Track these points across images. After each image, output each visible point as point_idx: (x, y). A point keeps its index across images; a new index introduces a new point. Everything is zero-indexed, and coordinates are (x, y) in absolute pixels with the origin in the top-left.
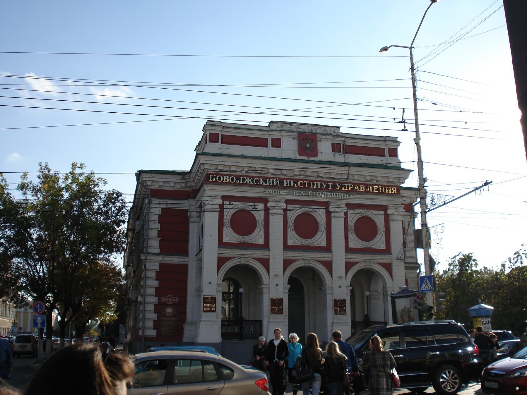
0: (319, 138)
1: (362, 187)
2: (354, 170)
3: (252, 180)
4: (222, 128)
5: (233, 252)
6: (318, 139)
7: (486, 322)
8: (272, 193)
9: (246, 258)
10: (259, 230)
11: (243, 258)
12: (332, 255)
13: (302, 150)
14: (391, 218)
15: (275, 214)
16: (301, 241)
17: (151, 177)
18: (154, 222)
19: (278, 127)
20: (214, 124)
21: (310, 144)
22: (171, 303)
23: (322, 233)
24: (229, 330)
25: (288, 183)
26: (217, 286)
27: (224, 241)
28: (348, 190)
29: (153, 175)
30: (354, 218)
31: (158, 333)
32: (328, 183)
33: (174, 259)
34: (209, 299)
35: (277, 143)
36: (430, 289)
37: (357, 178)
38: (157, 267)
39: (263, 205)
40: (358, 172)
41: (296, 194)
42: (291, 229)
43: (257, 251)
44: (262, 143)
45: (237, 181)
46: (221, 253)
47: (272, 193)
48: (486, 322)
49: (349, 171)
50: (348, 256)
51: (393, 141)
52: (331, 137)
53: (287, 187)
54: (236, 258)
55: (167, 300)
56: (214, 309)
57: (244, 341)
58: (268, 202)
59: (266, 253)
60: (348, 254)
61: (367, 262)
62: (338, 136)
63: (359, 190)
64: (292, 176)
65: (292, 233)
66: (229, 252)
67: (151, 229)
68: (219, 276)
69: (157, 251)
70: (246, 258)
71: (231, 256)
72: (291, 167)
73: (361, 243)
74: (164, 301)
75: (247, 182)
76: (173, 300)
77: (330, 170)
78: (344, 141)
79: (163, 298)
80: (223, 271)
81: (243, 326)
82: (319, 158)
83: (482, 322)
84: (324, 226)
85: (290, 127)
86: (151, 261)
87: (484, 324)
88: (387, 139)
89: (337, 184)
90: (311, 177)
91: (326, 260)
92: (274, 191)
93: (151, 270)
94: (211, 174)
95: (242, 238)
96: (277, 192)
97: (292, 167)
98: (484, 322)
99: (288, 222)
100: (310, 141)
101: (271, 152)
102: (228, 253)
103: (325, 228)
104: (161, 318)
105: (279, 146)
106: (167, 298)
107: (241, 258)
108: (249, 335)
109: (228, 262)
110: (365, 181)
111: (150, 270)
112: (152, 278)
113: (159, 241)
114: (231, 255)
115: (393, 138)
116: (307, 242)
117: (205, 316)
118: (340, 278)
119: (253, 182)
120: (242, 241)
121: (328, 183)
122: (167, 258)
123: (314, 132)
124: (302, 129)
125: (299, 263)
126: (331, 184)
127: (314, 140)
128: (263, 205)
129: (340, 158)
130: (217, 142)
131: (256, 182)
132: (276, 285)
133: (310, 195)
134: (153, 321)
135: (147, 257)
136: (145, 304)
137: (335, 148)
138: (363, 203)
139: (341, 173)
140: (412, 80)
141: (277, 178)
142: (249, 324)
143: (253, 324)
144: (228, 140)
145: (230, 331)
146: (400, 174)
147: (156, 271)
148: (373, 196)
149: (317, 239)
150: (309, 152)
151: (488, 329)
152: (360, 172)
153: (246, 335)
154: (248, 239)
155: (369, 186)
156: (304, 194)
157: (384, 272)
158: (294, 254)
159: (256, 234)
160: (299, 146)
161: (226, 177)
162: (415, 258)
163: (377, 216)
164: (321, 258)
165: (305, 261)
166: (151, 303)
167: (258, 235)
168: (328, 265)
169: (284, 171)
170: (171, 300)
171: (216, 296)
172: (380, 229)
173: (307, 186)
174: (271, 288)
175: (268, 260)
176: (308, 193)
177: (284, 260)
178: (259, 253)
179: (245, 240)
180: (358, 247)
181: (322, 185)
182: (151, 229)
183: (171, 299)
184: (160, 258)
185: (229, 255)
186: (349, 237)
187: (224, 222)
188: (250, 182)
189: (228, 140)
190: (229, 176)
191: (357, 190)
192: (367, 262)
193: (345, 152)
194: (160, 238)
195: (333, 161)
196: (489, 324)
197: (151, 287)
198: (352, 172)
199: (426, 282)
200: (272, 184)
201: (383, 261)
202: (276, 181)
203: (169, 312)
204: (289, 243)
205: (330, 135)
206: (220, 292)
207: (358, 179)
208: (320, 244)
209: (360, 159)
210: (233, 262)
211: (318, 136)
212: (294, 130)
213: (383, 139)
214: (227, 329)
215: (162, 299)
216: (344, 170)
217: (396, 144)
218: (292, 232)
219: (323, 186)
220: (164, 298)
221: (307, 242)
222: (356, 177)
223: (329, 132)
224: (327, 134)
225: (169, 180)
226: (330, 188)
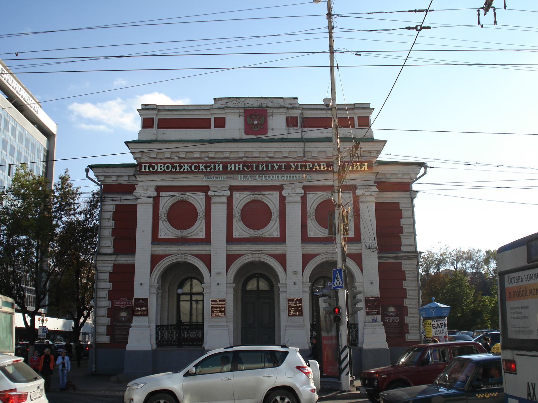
0: (269, 112)
1: (324, 165)
2: (310, 146)
3: (191, 167)
4: (157, 112)
5: (169, 248)
6: (269, 114)
7: (438, 324)
8: (212, 180)
9: (183, 254)
10: (200, 223)
11: (179, 255)
12: (286, 246)
13: (249, 128)
14: (213, 200)
15: (216, 203)
16: (249, 232)
17: (102, 172)
18: (108, 220)
19: (222, 104)
20: (149, 108)
21: (258, 120)
23: (274, 222)
24: (192, 335)
25: (358, 166)
26: (150, 287)
27: (159, 237)
28: (231, 171)
29: (105, 169)
30: (315, 203)
31: (111, 340)
32: (281, 164)
33: (128, 259)
34: (140, 302)
35: (221, 123)
36: (340, 285)
37: (316, 156)
38: (109, 268)
39: (278, 192)
40: (316, 148)
41: (241, 178)
42: (237, 219)
43: (196, 246)
44: (204, 124)
45: (173, 169)
46: (154, 250)
47: (212, 180)
48: (438, 324)
49: (304, 148)
50: (306, 247)
51: (365, 108)
52: (284, 110)
53: (231, 172)
54: (172, 256)
56: (146, 313)
58: (283, 189)
59: (207, 248)
60: (306, 245)
61: (330, 253)
62: (294, 108)
63: (205, 170)
64: (238, 159)
65: (238, 224)
66: (164, 248)
67: (105, 228)
68: (152, 277)
69: (111, 250)
70: (183, 254)
71: (167, 253)
72: (234, 149)
73: (323, 231)
75: (184, 169)
77: (281, 148)
78: (302, 114)
79: (116, 301)
80: (157, 270)
82: (270, 134)
83: (433, 325)
84: (277, 213)
85: (236, 103)
86: (104, 262)
87: (434, 327)
88: (356, 106)
89: (292, 164)
90: (260, 158)
91: (279, 253)
92: (215, 177)
93: (104, 272)
94: (144, 163)
95: (179, 232)
96: (218, 178)
97: (235, 148)
98: (434, 324)
99: (234, 211)
100: (258, 117)
101: (214, 133)
102: (163, 250)
103: (278, 216)
104: (114, 323)
105: (224, 126)
108: (163, 341)
109: (238, 260)
110: (327, 158)
112: (105, 281)
113: (112, 240)
114: (167, 252)
115: (364, 105)
116: (256, 233)
117: (135, 320)
118: (295, 273)
119: (191, 168)
120: (180, 235)
121: (281, 164)
122: (121, 258)
123: (265, 106)
124: (250, 104)
125: (247, 257)
126: (256, 165)
127: (262, 116)
128: (278, 192)
129: (295, 133)
130: (152, 127)
131: (195, 169)
132: (370, 283)
133: (257, 179)
134: (106, 326)
135: (97, 257)
136: (96, 308)
137: (291, 122)
138: (325, 184)
139: (280, 150)
140: (328, 29)
141: (220, 162)
142: (171, 329)
143: (167, 329)
144: (164, 124)
145: (193, 336)
146: (370, 146)
147: (110, 273)
148: (167, 177)
149: (268, 230)
150: (257, 129)
151: (441, 334)
152: (319, 148)
154: (186, 233)
155: (175, 165)
156: (251, 178)
157: (351, 264)
158: (240, 248)
159: (196, 227)
160: (245, 122)
161: (161, 166)
162: (414, 246)
163: (193, 197)
164: (273, 251)
165: (253, 255)
166: (104, 307)
167: (198, 227)
168: (282, 259)
169: (226, 154)
170: (125, 303)
171: (148, 298)
172: (165, 215)
173: (254, 169)
175: (360, 255)
176: (256, 177)
177: (302, 255)
178: (199, 248)
179: (183, 235)
180: (245, 237)
181: (273, 167)
182: (105, 228)
183: (124, 302)
184: (113, 258)
185: (165, 252)
186: (308, 224)
187: (159, 215)
188: (187, 169)
189: (164, 124)
190: (164, 164)
191: (316, 169)
192: (330, 253)
193: (303, 126)
194: (114, 237)
195: (286, 138)
196: (441, 327)
197: (103, 289)
198: (309, 148)
199: (338, 276)
200: (205, 169)
201: (350, 251)
202: (219, 165)
203: (123, 317)
204: (235, 236)
205: (284, 107)
206: (154, 294)
207: (317, 157)
208: (272, 235)
209: (322, 133)
210: (170, 259)
211: (269, 110)
212: (240, 106)
213: (352, 107)
214: (163, 335)
215: (115, 303)
216: (298, 147)
217: (368, 111)
218: (238, 223)
219: (275, 168)
220: (118, 301)
221: (256, 233)
222: (315, 154)
223: (283, 105)
224: (281, 107)
225: (122, 174)
226: (283, 169)
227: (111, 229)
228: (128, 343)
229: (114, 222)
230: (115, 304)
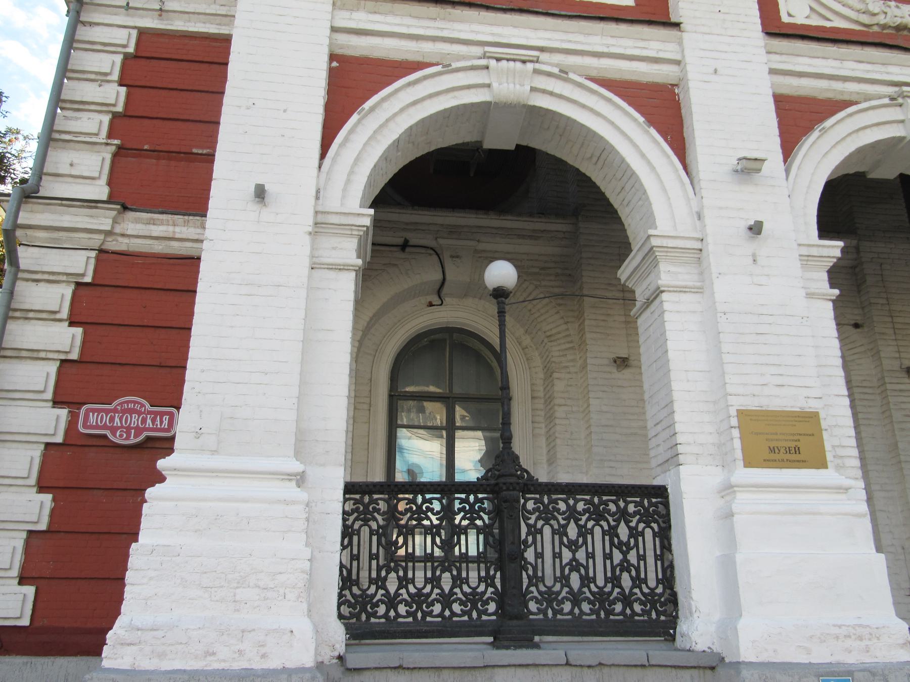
22: (133, 441)
55: (117, 420)
57: (537, 646)
74: (97, 427)
76: (149, 421)
79: (94, 410)
81: (524, 529)
106: (115, 411)
107: (493, 63)
111: (46, 277)
113: (108, 157)
143: (598, 515)
147: (78, 284)
153: (549, 597)
170: (135, 420)
174: (715, 258)
184: (103, 220)
194: (117, 142)
204: (790, 15)
220: (99, 411)
227: (121, 56)
228: (119, 614)
229: (123, 90)
230: (85, 426)
